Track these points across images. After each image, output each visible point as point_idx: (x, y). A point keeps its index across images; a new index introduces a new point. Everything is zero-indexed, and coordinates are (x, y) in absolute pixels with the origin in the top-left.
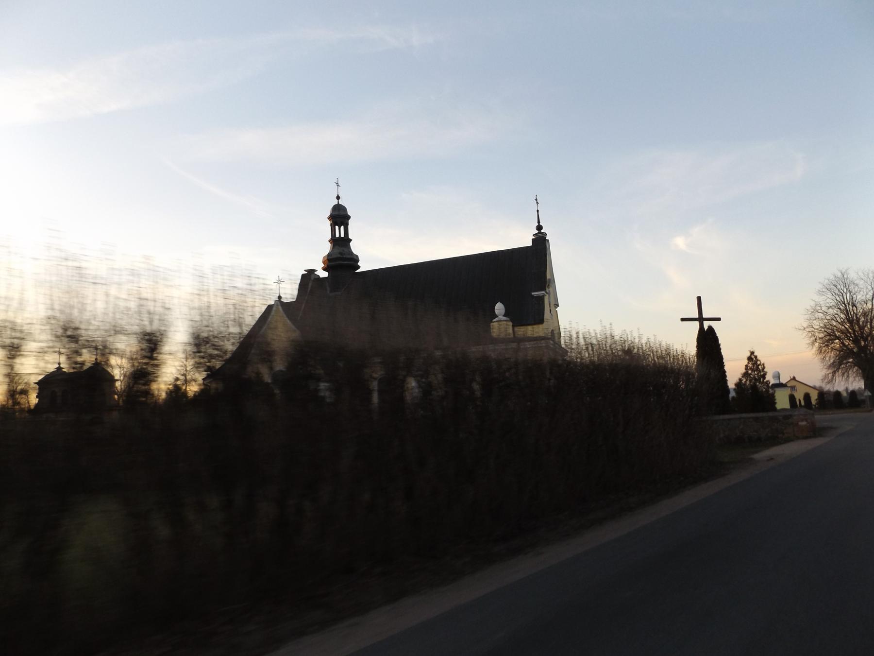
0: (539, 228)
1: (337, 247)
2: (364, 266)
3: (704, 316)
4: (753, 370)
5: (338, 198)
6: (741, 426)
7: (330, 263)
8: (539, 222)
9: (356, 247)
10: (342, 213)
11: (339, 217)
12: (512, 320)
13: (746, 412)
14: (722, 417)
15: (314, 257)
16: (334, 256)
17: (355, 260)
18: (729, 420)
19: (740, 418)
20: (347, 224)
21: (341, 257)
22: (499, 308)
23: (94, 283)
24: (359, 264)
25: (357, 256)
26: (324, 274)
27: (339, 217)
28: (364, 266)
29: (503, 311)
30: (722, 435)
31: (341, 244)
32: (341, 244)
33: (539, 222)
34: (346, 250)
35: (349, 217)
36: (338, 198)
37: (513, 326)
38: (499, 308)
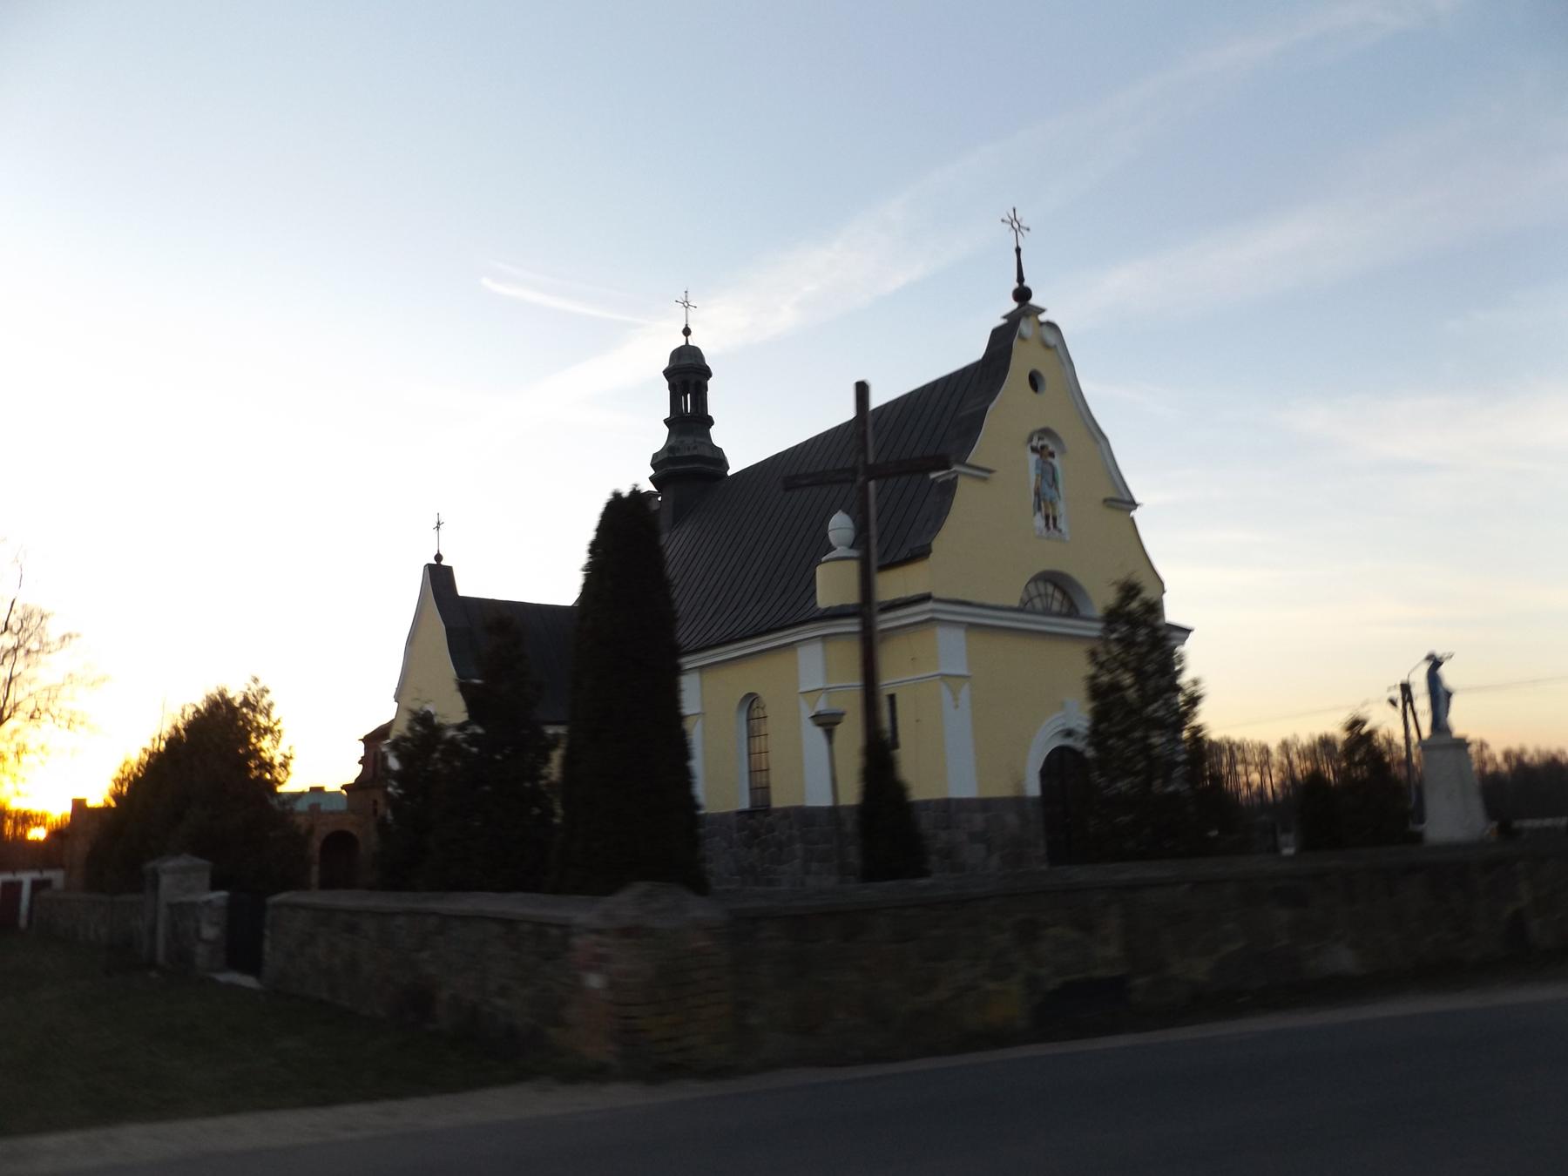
2: (737, 463)
5: (687, 332)
8: (1021, 279)
10: (686, 361)
11: (688, 374)
22: (840, 526)
27: (688, 374)
28: (737, 463)
33: (1021, 279)
35: (707, 373)
36: (687, 332)
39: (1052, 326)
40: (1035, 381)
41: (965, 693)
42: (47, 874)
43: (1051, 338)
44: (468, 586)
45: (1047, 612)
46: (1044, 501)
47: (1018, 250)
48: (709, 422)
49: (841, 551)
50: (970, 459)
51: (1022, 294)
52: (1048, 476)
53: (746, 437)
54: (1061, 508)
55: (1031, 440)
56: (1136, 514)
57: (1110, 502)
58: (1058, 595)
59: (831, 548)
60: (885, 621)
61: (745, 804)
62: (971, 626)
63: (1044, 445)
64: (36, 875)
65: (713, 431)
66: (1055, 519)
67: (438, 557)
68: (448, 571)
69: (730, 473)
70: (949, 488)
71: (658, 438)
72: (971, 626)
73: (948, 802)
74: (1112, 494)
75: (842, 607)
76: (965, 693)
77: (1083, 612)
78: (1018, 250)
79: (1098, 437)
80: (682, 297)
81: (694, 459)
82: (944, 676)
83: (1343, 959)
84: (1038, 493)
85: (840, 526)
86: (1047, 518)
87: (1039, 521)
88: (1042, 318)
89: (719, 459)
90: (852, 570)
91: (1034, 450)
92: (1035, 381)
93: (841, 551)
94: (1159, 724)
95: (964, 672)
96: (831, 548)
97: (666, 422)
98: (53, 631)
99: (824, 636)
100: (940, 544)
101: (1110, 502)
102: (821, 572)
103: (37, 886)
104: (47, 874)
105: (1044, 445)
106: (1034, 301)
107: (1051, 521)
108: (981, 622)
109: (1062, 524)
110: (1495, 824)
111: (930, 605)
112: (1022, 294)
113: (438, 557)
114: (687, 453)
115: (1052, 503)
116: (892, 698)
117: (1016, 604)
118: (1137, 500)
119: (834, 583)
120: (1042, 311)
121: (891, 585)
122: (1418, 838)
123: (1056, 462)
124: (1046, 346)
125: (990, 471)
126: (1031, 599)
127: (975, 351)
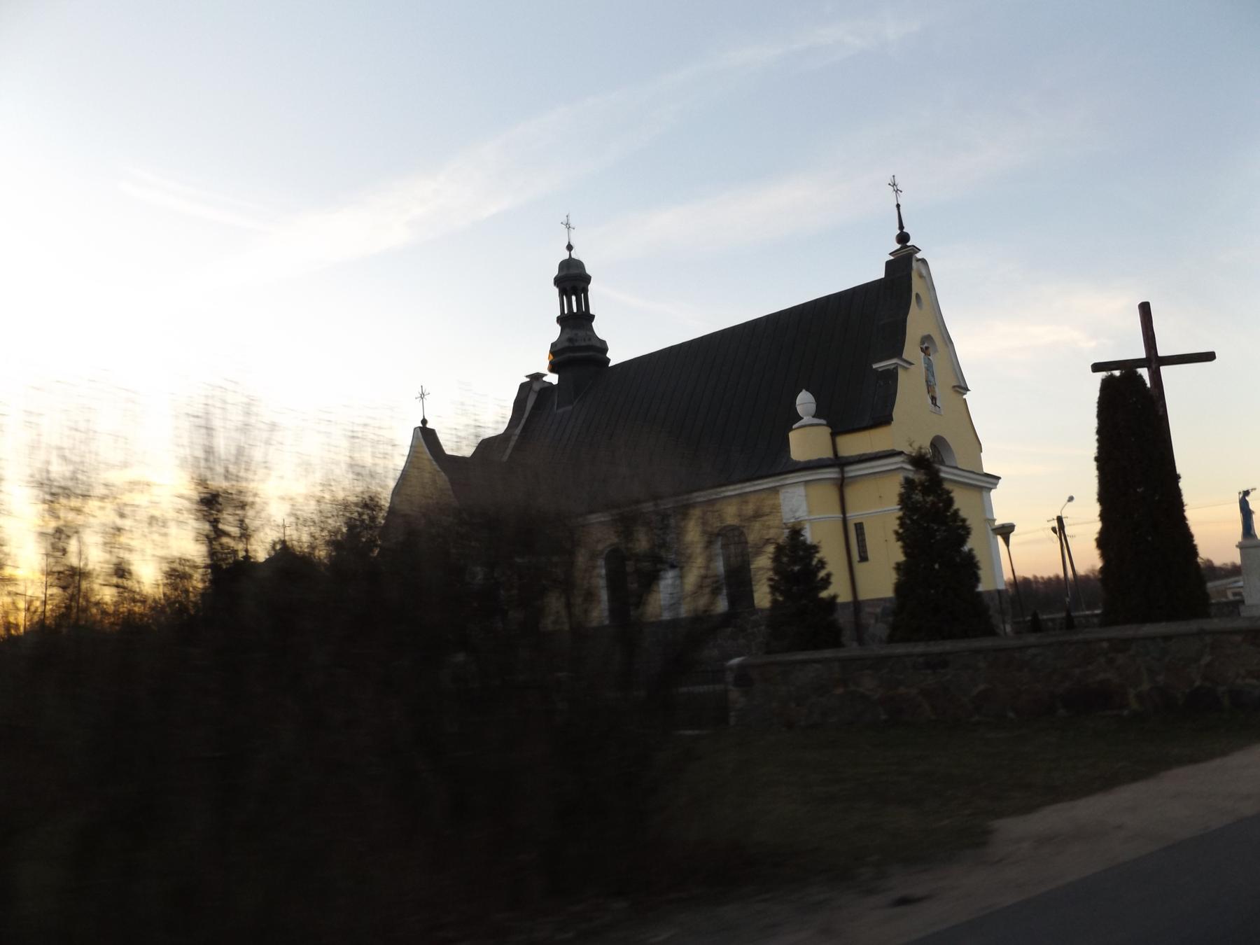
0: (903, 238)
1: (567, 330)
2: (616, 356)
3: (1162, 351)
4: (926, 491)
5: (570, 248)
6: (1207, 659)
7: (561, 357)
8: (901, 227)
9: (600, 328)
10: (574, 271)
11: (572, 280)
12: (828, 425)
13: (1170, 618)
14: (1149, 629)
15: (531, 352)
16: (559, 347)
17: (602, 348)
18: (1167, 638)
19: (1201, 633)
20: (585, 291)
21: (577, 346)
22: (805, 401)
23: (76, 430)
24: (608, 355)
25: (604, 342)
26: (553, 379)
27: (572, 280)
28: (616, 356)
29: (813, 407)
30: (1145, 687)
31: (576, 321)
32: (576, 321)
33: (901, 227)
34: (581, 333)
35: (587, 279)
36: (570, 248)
37: (834, 435)
38: (805, 401)
43: (924, 272)
47: (898, 206)
48: (591, 318)
60: (852, 471)
65: (595, 325)
67: (424, 421)
68: (432, 432)
69: (611, 364)
72: (956, 468)
75: (820, 460)
78: (898, 206)
81: (581, 349)
93: (807, 420)
94: (960, 527)
97: (592, 317)
99: (806, 482)
102: (793, 436)
105: (927, 345)
110: (208, 561)
112: (903, 238)
113: (424, 421)
114: (583, 344)
119: (807, 441)
125: (911, 364)
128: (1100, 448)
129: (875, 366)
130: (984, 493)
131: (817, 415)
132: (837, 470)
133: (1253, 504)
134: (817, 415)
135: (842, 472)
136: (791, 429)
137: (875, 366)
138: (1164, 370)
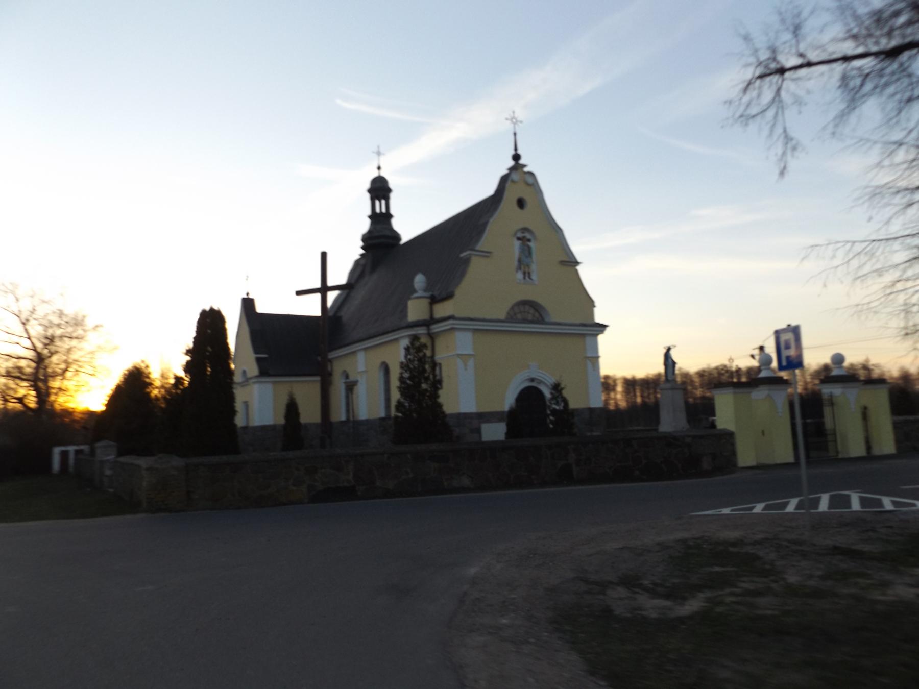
5: (379, 168)
8: (516, 149)
11: (380, 189)
21: (380, 239)
22: (419, 280)
27: (380, 189)
32: (381, 221)
33: (516, 149)
36: (379, 168)
39: (531, 174)
40: (521, 203)
41: (471, 363)
42: (82, 447)
43: (530, 180)
44: (260, 308)
45: (525, 321)
46: (523, 265)
47: (515, 134)
49: (420, 293)
50: (478, 247)
51: (516, 157)
52: (526, 251)
53: (409, 225)
54: (534, 267)
55: (515, 234)
56: (579, 268)
57: (563, 263)
58: (532, 311)
59: (415, 291)
60: (436, 328)
61: (382, 414)
62: (475, 331)
63: (524, 238)
64: (75, 447)
66: (529, 273)
70: (467, 261)
71: (365, 225)
73: (460, 414)
74: (565, 258)
75: (418, 321)
76: (471, 363)
77: (547, 320)
78: (515, 134)
79: (556, 230)
80: (375, 149)
82: (459, 355)
83: (466, 481)
84: (520, 261)
85: (419, 280)
86: (524, 273)
87: (520, 275)
88: (526, 170)
89: (397, 237)
90: (425, 303)
91: (519, 239)
92: (521, 203)
95: (471, 352)
96: (415, 291)
98: (89, 323)
100: (459, 292)
101: (563, 263)
103: (77, 452)
104: (82, 447)
105: (524, 238)
106: (522, 162)
107: (527, 274)
108: (480, 326)
109: (534, 277)
111: (451, 321)
112: (516, 157)
115: (528, 266)
116: (246, 404)
117: (503, 317)
118: (579, 260)
119: (416, 310)
120: (525, 166)
121: (442, 310)
122: (713, 425)
123: (531, 244)
124: (528, 184)
126: (515, 314)
127: (488, 190)
128: (197, 340)
129: (462, 255)
130: (588, 340)
131: (425, 290)
132: (425, 328)
133: (674, 355)
134: (425, 290)
135: (429, 329)
136: (409, 298)
137: (462, 255)
138: (330, 283)
